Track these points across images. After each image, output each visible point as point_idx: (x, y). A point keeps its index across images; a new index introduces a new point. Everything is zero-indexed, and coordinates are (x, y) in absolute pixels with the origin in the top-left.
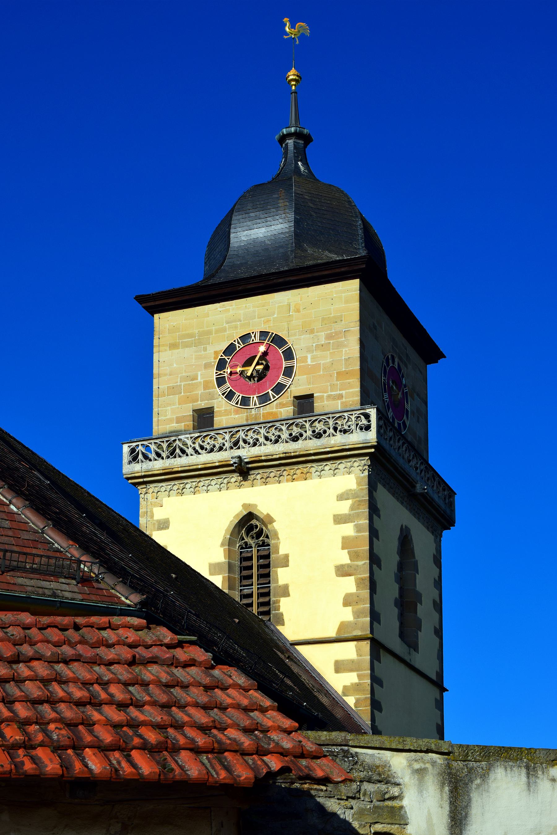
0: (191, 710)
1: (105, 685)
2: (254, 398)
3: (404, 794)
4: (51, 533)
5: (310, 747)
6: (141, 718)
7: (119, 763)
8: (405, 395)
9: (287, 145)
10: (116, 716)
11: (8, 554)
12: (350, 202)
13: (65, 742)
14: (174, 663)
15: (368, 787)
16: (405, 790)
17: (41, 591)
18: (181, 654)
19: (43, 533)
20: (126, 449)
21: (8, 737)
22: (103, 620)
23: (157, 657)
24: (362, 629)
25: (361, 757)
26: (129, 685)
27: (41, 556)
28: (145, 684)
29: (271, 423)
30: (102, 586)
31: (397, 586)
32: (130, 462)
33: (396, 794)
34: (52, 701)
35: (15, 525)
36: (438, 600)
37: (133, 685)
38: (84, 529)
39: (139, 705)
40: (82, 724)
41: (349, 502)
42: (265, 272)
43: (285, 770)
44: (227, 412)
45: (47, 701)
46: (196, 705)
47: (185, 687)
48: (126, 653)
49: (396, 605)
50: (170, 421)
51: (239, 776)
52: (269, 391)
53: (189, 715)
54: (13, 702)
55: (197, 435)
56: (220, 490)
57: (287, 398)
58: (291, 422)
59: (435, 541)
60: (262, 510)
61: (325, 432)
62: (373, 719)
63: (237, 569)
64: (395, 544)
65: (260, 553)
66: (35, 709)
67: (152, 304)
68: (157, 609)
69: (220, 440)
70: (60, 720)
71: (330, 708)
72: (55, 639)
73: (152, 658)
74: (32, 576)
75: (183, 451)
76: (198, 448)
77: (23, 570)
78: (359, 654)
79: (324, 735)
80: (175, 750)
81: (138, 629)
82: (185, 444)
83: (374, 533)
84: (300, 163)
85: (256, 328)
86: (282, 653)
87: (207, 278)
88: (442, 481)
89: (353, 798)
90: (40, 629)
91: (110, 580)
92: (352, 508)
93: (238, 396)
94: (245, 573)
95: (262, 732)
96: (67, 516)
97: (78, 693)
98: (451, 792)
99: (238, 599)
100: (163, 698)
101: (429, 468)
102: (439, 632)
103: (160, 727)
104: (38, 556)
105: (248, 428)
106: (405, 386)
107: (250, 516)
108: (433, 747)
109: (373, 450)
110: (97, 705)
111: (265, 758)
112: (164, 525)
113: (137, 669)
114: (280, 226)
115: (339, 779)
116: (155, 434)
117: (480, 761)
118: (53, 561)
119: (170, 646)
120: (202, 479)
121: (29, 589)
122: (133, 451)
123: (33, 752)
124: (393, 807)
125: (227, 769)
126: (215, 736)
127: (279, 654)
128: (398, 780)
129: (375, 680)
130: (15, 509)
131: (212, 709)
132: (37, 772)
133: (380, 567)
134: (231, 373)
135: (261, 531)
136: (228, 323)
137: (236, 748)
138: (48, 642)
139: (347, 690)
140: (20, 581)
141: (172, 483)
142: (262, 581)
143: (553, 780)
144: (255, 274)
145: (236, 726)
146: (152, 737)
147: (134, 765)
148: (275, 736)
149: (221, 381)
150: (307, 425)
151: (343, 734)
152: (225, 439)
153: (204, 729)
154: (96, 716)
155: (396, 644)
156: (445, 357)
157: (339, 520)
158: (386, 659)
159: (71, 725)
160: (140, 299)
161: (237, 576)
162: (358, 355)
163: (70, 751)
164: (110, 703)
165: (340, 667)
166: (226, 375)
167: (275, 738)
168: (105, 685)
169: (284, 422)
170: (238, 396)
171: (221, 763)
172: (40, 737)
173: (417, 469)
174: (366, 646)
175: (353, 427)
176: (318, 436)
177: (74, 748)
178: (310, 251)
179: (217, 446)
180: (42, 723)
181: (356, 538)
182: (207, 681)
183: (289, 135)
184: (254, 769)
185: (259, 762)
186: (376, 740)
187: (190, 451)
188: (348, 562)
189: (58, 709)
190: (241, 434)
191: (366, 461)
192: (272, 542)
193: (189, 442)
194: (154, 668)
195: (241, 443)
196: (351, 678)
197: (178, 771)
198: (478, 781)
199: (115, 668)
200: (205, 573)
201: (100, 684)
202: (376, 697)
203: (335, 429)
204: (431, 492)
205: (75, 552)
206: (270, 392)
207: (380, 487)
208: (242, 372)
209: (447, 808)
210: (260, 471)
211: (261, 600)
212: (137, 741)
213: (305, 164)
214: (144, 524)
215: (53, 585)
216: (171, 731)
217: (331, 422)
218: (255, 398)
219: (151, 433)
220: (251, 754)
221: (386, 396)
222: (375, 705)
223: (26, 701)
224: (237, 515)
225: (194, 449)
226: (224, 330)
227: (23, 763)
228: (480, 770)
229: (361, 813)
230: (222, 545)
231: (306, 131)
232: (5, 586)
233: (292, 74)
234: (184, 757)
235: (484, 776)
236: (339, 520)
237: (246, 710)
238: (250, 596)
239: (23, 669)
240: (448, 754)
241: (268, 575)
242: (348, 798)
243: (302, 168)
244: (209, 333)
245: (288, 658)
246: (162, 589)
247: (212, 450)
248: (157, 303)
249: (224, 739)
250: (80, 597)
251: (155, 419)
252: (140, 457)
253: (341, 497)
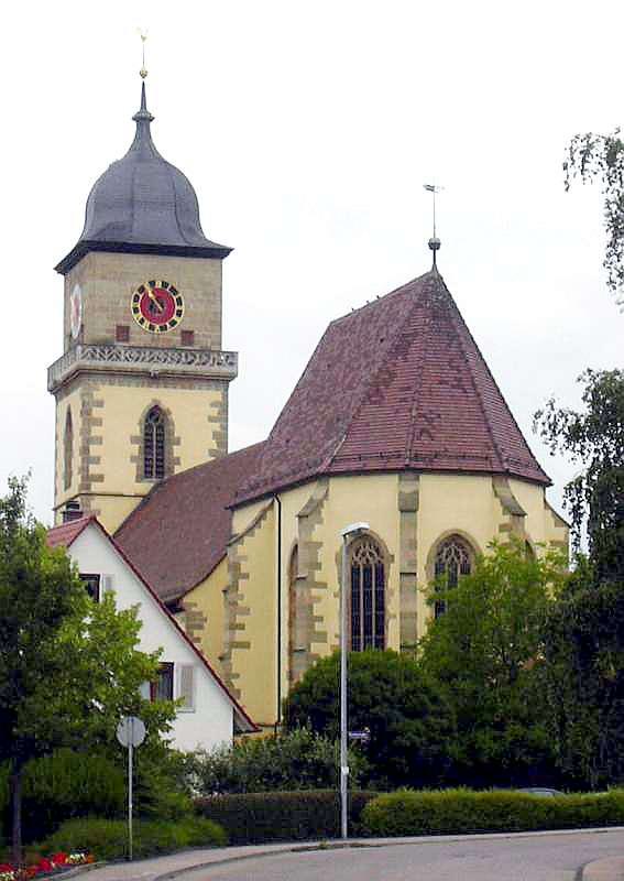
60: (165, 405)
184: (136, 608)
253: (212, 405)
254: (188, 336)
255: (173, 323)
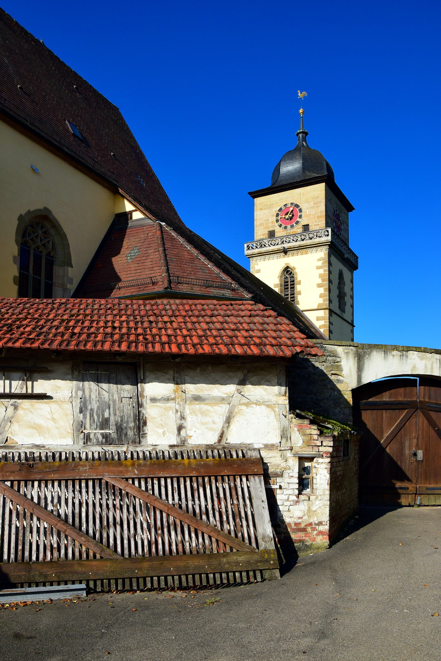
0: (270, 332)
1: (241, 324)
2: (289, 226)
3: (342, 360)
4: (222, 274)
5: (310, 344)
6: (254, 334)
7: (246, 349)
8: (341, 223)
9: (299, 136)
10: (245, 334)
11: (208, 282)
12: (321, 155)
13: (229, 343)
14: (264, 316)
15: (329, 358)
16: (342, 359)
17: (219, 294)
18: (266, 313)
19: (219, 274)
20: (246, 245)
21: (210, 341)
22: (240, 302)
23: (258, 314)
24: (326, 306)
25: (327, 348)
26: (249, 324)
27: (219, 282)
28: (255, 323)
29: (295, 235)
30: (239, 291)
31: (338, 291)
32: (247, 250)
33: (339, 361)
34: (224, 329)
35: (210, 272)
36: (352, 295)
37: (251, 324)
38: (233, 273)
39: (253, 330)
40: (234, 337)
41: (322, 262)
42: (292, 182)
43: (302, 352)
44: (280, 232)
45: (223, 329)
46: (272, 330)
47: (268, 324)
48: (248, 313)
49: (337, 297)
50: (260, 235)
51: (287, 354)
52: (294, 224)
53: (269, 333)
54: (211, 330)
55: (269, 240)
56: (277, 258)
57: (300, 225)
58: (301, 234)
59: (351, 275)
60: (291, 265)
61: (313, 237)
62: (329, 337)
63: (283, 286)
64: (337, 276)
65: (291, 280)
66: (219, 332)
67: (254, 195)
68: (257, 299)
69: (277, 242)
70: (227, 336)
71: (315, 333)
72: (225, 309)
73: (257, 314)
74: (216, 289)
75: (265, 246)
76: (270, 244)
77: (213, 287)
78: (325, 314)
79: (314, 341)
80: (265, 345)
81: (252, 305)
82: (265, 243)
83: (330, 272)
84: (304, 142)
85: (289, 202)
86: (299, 314)
87: (272, 185)
88: (353, 253)
89: (324, 362)
90: (220, 305)
91: (241, 289)
92: (322, 264)
93: (283, 226)
94: (286, 287)
95: (294, 339)
96: (227, 269)
97: (233, 327)
98: (358, 360)
99: (284, 296)
100: (261, 328)
101: (349, 249)
102: (352, 306)
103: (260, 338)
104: (218, 282)
105: (287, 237)
106: (341, 220)
107: (288, 267)
108: (352, 344)
109: (330, 243)
110: (239, 330)
111: (295, 348)
112: (258, 271)
113: (252, 318)
114: (297, 165)
115: (320, 355)
116: (255, 240)
117: (368, 349)
118: (222, 284)
119: (262, 311)
120: (271, 255)
121: (215, 293)
122: (248, 246)
123: (218, 346)
124: (338, 365)
125: (282, 351)
126: (278, 340)
127: (298, 314)
128: (339, 356)
129: (330, 323)
130: (210, 266)
131: (277, 331)
132: (220, 353)
133: (332, 284)
134: (281, 218)
135: (291, 272)
136: (279, 200)
137: (286, 344)
138: (222, 310)
139: (321, 327)
140: (212, 290)
141: (261, 257)
142: (292, 289)
143: (393, 356)
144: (289, 183)
145: (285, 337)
146: (257, 341)
147: (252, 350)
148: (298, 340)
149: (277, 221)
150: (307, 235)
151: (321, 340)
152: (279, 241)
153: (274, 338)
154: (238, 334)
155: (337, 310)
156: (355, 209)
157: (318, 268)
158: (334, 316)
159: (231, 337)
160: (250, 193)
161: (283, 288)
162: (325, 210)
163: (230, 346)
164: (243, 330)
165: (318, 319)
166: (279, 219)
167: (299, 341)
168: (241, 324)
169: (299, 234)
170: (283, 226)
171: (281, 349)
172: (220, 341)
173: (345, 249)
174: (327, 311)
175: (323, 235)
176: (311, 239)
177: (232, 345)
178: (308, 174)
179: (276, 244)
180: (221, 337)
181: (324, 274)
182: (275, 322)
183: (300, 133)
184: (292, 351)
185: (293, 349)
186: (332, 342)
187: (267, 245)
188: (321, 282)
189: (226, 332)
190: (284, 239)
191: (327, 247)
192: (295, 276)
193: (267, 243)
194: (257, 318)
195: (284, 242)
196: (322, 323)
197: (266, 352)
198: (367, 356)
199: (244, 318)
200: (272, 287)
201: (240, 323)
202: (331, 329)
203: (317, 236)
204: (350, 257)
205: (230, 280)
206: (294, 224)
207: (332, 256)
208: (284, 218)
209: (356, 365)
210: (291, 252)
211: (292, 296)
212: (252, 342)
213: (306, 143)
214: (252, 271)
215: (223, 292)
216: (263, 339)
217: (315, 234)
218: (289, 226)
219: (254, 240)
220: (291, 346)
221: (334, 224)
222: (330, 332)
223: (216, 330)
224: (283, 267)
225: (269, 245)
226: (278, 203)
227: (215, 350)
228: (368, 352)
229: (327, 367)
230: (278, 277)
231: (306, 131)
232: (207, 292)
233: (301, 111)
234: (268, 347)
235: (369, 355)
236: (318, 268)
237: (288, 332)
238: (288, 295)
239: (214, 319)
240: (357, 347)
241: (294, 288)
242: (322, 362)
243: (305, 144)
244: (273, 204)
245: (301, 316)
246: (258, 293)
247: (274, 245)
248: (255, 194)
249: (281, 341)
250: (232, 295)
251: (255, 235)
252: (250, 248)
253: (319, 260)
254: (306, 227)
255: (297, 223)
